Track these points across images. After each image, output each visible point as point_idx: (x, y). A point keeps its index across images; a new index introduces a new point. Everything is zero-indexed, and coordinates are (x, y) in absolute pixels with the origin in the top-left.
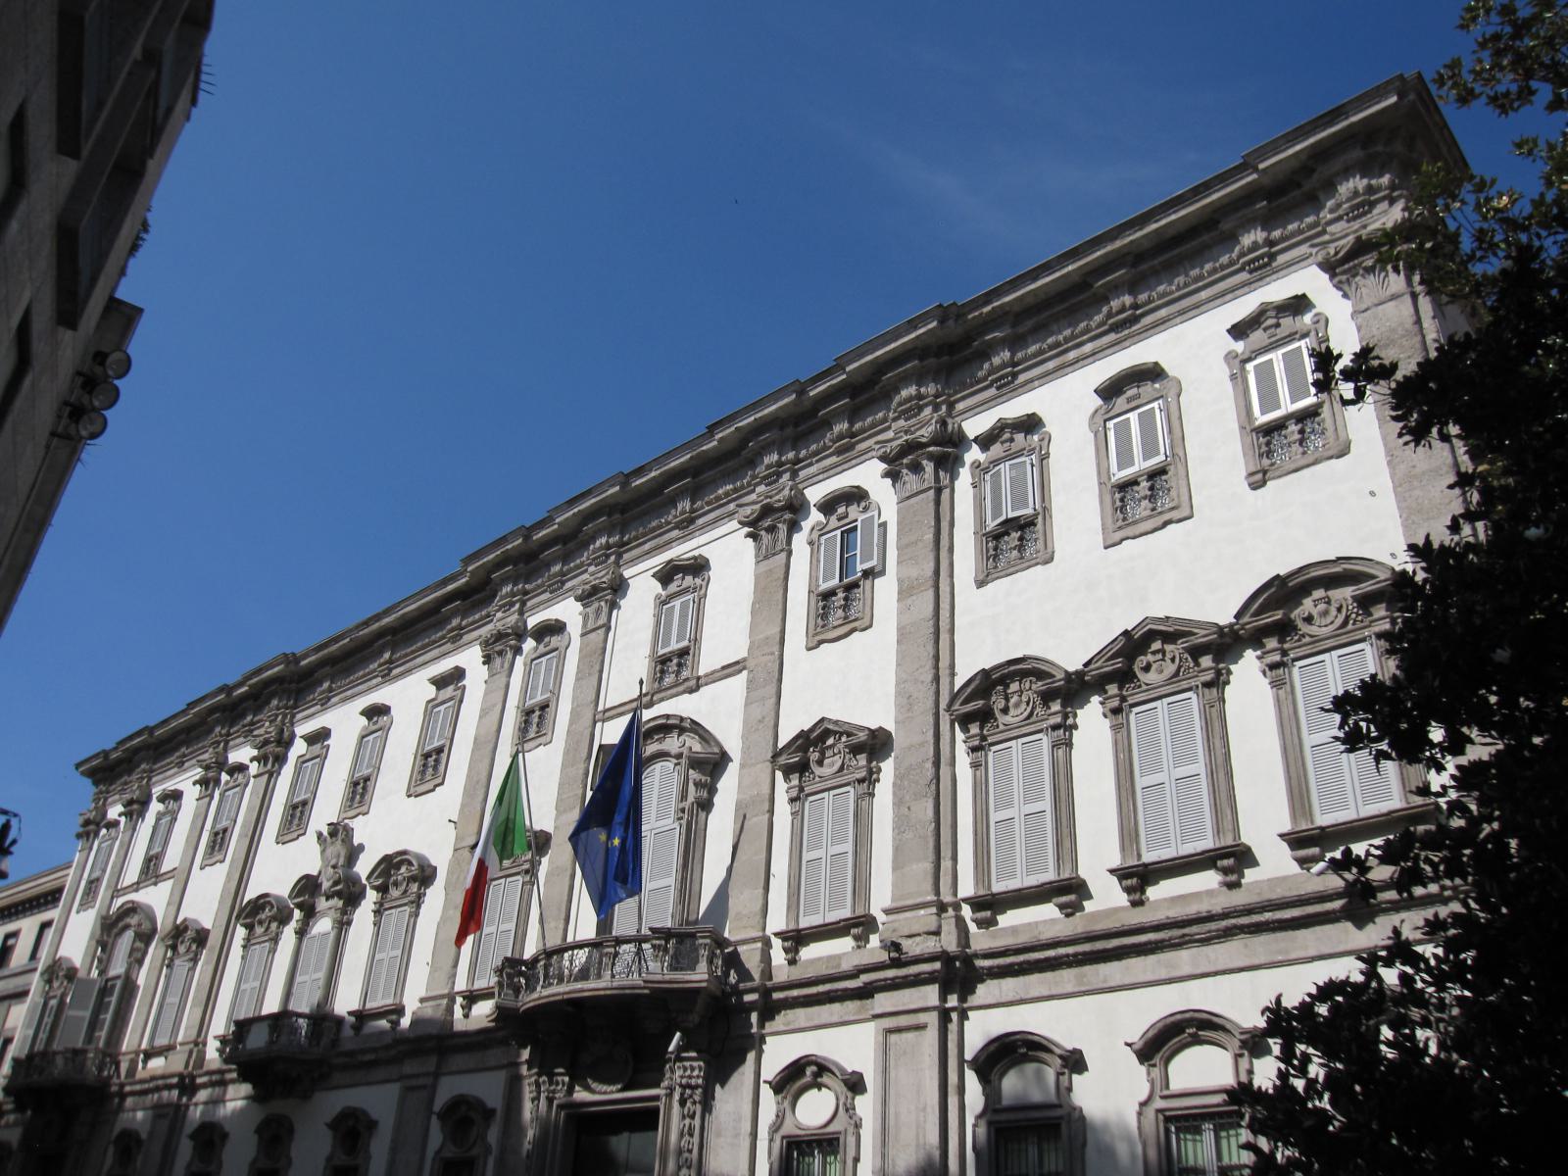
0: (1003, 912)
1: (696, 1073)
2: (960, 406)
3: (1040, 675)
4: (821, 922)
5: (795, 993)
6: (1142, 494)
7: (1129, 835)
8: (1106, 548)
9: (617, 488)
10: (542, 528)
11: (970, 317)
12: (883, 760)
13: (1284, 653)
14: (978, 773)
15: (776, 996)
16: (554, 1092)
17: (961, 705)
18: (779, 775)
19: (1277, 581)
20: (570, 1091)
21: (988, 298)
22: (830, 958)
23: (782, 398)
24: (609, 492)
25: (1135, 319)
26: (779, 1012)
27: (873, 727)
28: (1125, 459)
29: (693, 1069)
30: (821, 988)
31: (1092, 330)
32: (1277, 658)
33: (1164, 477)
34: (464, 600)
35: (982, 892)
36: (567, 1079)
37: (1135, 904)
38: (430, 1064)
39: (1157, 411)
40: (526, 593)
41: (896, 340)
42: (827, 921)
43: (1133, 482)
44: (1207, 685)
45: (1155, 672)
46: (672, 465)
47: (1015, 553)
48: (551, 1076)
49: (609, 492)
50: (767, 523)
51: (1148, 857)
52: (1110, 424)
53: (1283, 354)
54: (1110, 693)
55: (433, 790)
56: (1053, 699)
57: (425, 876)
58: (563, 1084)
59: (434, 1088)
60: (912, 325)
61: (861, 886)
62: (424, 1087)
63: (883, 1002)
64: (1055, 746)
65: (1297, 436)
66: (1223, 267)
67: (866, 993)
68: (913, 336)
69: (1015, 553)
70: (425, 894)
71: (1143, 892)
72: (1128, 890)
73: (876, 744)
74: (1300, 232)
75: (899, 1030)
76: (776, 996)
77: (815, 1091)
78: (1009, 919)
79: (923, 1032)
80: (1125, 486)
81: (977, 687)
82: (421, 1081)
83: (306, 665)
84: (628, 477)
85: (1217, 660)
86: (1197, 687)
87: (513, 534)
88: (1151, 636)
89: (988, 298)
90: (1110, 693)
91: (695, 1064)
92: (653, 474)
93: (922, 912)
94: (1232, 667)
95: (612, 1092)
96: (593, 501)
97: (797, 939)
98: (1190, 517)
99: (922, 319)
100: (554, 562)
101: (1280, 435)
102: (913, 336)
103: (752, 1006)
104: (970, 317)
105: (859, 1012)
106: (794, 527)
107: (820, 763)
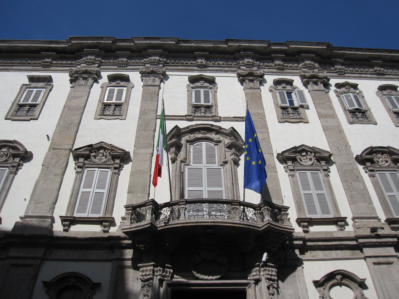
0: (312, 226)
1: (168, 274)
2: (102, 67)
3: (15, 148)
4: (86, 216)
5: (320, 243)
6: (25, 110)
7: (71, 206)
8: (6, 119)
9: (175, 43)
10: (124, 42)
11: (334, 51)
12: (26, 162)
13: (84, 164)
14: (79, 176)
15: (308, 244)
16: (164, 276)
17: (366, 155)
18: (71, 158)
19: (372, 148)
20: (172, 277)
21: (341, 49)
22: (326, 233)
23: (262, 44)
24: (169, 42)
25: (283, 70)
26: (307, 251)
27: (28, 150)
28: (27, 99)
29: (272, 271)
30: (334, 243)
31: (293, 67)
32: (81, 165)
33: (35, 108)
34: (57, 53)
35: (69, 215)
36: (172, 271)
37: (65, 230)
38: (40, 252)
39: (43, 91)
40: (101, 62)
41: (311, 46)
42: (89, 216)
43: (109, 105)
44: (115, 168)
45: (101, 158)
46: (203, 45)
47: (25, 112)
48: (164, 267)
49: (169, 42)
50: (85, 76)
51: (76, 215)
52: (108, 88)
53: (110, 89)
54: (80, 161)
55: (29, 120)
56: (17, 157)
57: (27, 157)
58: (170, 273)
59: (38, 269)
60: (318, 44)
61: (110, 207)
62: (31, 265)
63: (368, 251)
64: (11, 173)
65: (27, 110)
66: (59, 64)
67: (359, 248)
68: (318, 47)
69: (25, 112)
70: (22, 165)
71: (69, 227)
72: (64, 226)
73: (123, 157)
74: (56, 64)
75: (17, 265)
76: (308, 244)
77: (338, 287)
78: (314, 229)
79: (391, 265)
80: (21, 106)
81: (370, 151)
82: (33, 262)
83: (273, 48)
84: (179, 41)
85: (121, 162)
86: (112, 168)
87: (108, 38)
88: (101, 148)
89: (341, 49)
90: (80, 161)
91: (273, 269)
92: (192, 45)
93: (372, 220)
94: (124, 165)
95: (212, 280)
96: (159, 42)
97: (69, 221)
98: (125, 119)
99: (322, 44)
100: (123, 57)
101: (34, 108)
102: (318, 47)
103: (297, 246)
104: (334, 51)
105: (352, 255)
106: (96, 81)
107: (95, 157)
